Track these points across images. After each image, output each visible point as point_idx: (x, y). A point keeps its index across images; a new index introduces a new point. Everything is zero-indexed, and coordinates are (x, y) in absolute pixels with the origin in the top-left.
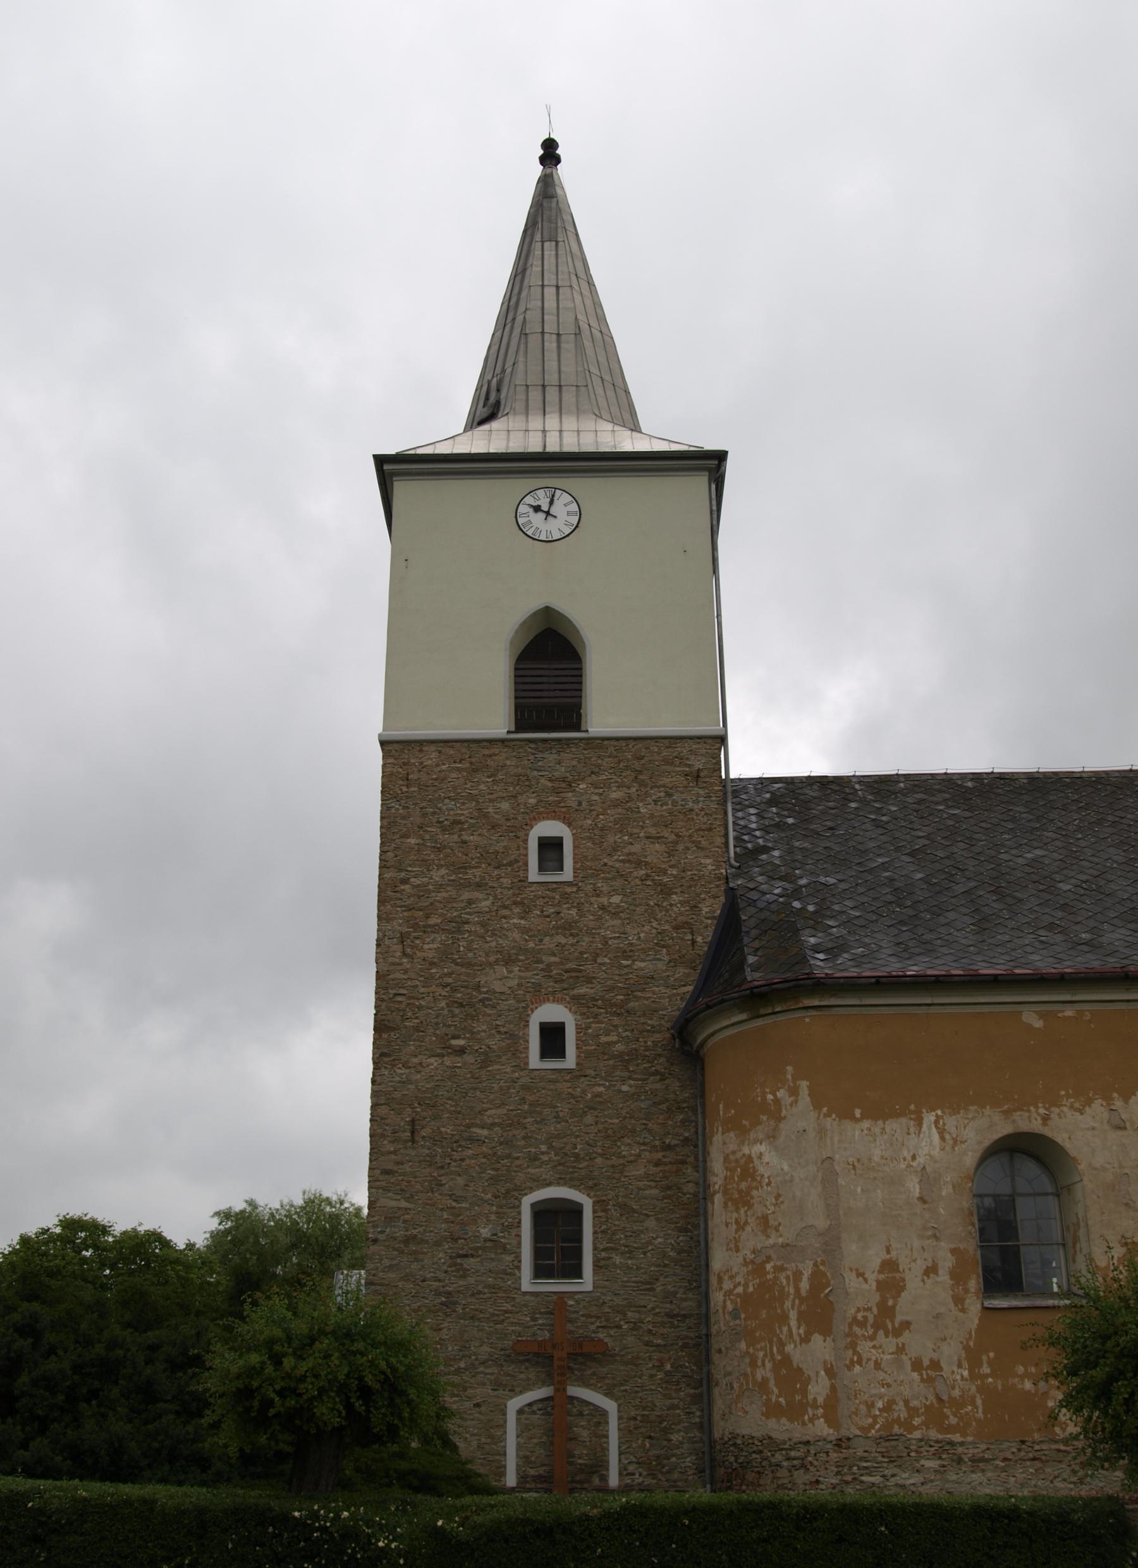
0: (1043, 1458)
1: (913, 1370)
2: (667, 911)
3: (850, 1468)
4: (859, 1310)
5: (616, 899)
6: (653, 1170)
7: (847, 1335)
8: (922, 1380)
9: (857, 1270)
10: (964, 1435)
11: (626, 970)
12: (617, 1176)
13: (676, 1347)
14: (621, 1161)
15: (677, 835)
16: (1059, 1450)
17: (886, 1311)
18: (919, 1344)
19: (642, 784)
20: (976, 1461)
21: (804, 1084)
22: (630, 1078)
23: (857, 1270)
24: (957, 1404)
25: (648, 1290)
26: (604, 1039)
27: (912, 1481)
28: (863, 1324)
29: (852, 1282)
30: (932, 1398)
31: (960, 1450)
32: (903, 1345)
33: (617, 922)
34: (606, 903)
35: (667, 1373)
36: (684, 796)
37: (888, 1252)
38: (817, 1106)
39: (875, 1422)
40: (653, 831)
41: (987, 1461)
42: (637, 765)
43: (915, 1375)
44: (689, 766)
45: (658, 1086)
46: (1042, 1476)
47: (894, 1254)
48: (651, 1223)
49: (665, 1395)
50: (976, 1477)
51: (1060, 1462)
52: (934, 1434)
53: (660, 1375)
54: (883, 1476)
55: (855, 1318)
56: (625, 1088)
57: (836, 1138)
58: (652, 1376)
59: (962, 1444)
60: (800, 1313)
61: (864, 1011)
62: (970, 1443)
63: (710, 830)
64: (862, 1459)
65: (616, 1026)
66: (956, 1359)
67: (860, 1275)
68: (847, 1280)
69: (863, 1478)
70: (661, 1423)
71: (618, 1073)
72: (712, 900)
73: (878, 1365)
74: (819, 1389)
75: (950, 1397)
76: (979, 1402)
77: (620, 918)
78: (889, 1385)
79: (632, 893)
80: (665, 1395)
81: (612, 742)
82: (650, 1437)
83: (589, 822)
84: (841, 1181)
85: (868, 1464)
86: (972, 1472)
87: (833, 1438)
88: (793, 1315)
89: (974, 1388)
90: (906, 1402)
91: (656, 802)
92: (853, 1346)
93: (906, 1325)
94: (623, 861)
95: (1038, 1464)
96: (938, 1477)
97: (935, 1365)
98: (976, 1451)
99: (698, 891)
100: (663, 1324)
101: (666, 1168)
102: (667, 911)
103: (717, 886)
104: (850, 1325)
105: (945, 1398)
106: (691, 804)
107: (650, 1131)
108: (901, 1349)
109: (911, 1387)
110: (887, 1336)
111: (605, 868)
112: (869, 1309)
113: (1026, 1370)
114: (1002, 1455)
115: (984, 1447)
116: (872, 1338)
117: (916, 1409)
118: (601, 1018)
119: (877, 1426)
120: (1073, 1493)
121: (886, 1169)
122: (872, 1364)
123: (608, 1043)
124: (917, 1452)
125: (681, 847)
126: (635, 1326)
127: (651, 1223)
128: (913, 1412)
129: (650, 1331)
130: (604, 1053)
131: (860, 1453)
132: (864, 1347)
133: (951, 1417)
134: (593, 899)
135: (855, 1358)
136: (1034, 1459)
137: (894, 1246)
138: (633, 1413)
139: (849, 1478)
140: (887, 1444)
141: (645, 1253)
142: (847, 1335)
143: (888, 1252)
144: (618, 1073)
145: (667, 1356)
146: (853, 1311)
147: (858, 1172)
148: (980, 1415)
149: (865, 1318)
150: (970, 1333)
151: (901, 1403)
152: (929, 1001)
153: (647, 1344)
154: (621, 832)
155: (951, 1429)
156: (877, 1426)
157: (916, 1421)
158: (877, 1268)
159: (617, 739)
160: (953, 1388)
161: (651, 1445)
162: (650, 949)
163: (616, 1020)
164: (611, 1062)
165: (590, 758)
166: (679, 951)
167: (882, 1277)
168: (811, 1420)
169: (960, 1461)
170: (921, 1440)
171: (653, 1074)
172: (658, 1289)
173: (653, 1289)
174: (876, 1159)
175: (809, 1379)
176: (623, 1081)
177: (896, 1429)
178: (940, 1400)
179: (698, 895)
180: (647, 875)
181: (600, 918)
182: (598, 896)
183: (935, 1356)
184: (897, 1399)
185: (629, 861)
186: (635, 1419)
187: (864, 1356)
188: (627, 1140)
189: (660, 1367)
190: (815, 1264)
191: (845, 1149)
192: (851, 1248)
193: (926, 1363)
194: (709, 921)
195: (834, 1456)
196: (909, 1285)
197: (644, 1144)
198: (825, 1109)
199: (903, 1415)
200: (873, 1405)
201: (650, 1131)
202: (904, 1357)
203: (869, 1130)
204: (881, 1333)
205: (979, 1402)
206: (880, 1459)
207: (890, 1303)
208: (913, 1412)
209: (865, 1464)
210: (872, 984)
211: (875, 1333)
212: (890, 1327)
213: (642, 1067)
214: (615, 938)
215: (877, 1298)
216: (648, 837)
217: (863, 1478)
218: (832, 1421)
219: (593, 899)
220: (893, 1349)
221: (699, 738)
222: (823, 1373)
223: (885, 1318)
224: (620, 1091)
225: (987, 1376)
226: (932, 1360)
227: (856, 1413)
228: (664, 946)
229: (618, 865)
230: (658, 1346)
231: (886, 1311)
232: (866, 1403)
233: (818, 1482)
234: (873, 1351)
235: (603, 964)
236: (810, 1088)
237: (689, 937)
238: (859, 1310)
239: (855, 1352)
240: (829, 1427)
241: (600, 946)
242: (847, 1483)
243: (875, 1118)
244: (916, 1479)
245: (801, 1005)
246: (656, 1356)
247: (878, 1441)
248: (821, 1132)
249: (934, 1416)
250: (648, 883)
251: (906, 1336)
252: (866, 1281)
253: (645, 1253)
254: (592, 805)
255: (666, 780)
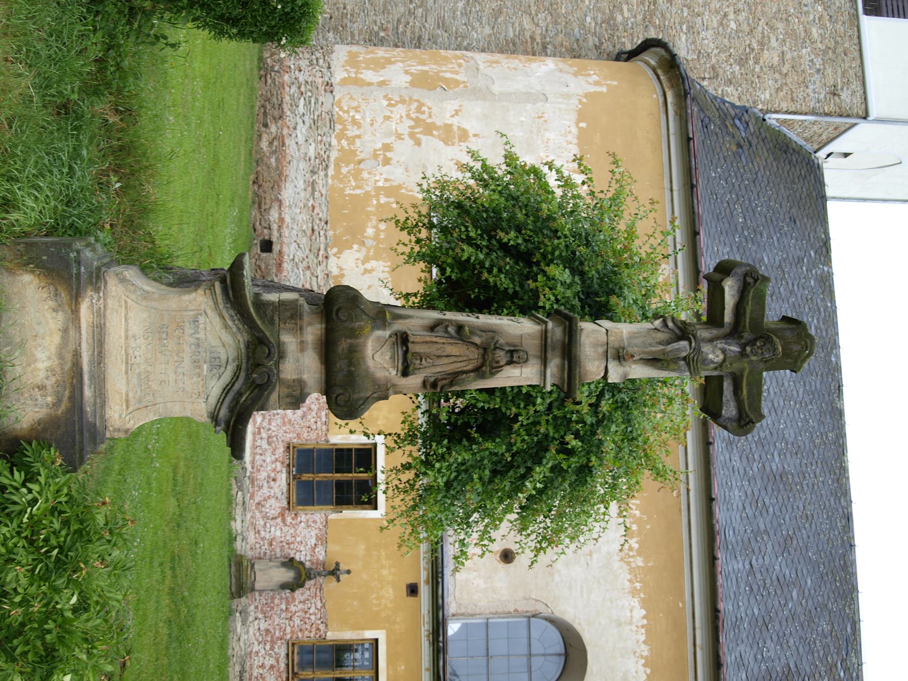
0: (314, 237)
1: (383, 144)
2: (726, 61)
3: (311, 91)
4: (430, 108)
5: (733, 25)
6: (528, 35)
7: (410, 98)
8: (375, 151)
9: (460, 110)
10: (333, 177)
11: (678, 28)
12: (522, 8)
13: (396, 40)
14: (533, 12)
15: (786, 75)
16: (319, 250)
17: (429, 129)
18: (403, 150)
19: (825, 52)
20: (313, 184)
21: (604, 89)
22: (596, 23)
23: (460, 110)
24: (357, 174)
25: (439, 24)
26: (625, 7)
27: (299, 135)
28: (419, 110)
29: (451, 105)
30: (361, 156)
31: (322, 173)
32: (403, 139)
33: (715, 24)
34: (729, 17)
35: (377, 34)
36: (818, 82)
37: (475, 135)
38: (587, 95)
39: (344, 112)
40: (788, 56)
41: (313, 194)
42: (840, 50)
43: (379, 145)
44: (842, 89)
45: (591, 43)
46: (300, 234)
47: (473, 139)
48: (487, 30)
49: (361, 30)
50: (301, 184)
51: (310, 250)
52: (334, 155)
53: (376, 28)
54: (303, 114)
55: (423, 105)
56: (588, 19)
57: (562, 106)
58: (375, 22)
59: (326, 175)
60: (427, 71)
61: (665, 139)
62: (327, 181)
63: (792, 100)
64: (317, 99)
65: (635, 17)
66: (392, 177)
67: (457, 112)
68: (453, 102)
69: (302, 99)
70: (341, 26)
71: (600, 15)
72: (737, 95)
73: (387, 118)
74: (369, 75)
75: (362, 170)
76: (358, 192)
77: (718, 27)
78: (372, 125)
79: (738, 37)
80: (361, 30)
81: (856, 33)
82: (331, 18)
83: (792, 11)
84: (529, 106)
85: (313, 104)
86: (305, 181)
87: (333, 80)
88: (425, 68)
89: (368, 189)
90: (359, 137)
91: (812, 61)
92: (403, 101)
93: (418, 143)
94: (763, 33)
95: (309, 232)
96: (302, 155)
97: (387, 161)
98: (321, 186)
99: (743, 86)
100: (413, 33)
101: (529, 44)
102: (726, 61)
103: (748, 101)
104: (418, 101)
105: (362, 166)
106: (812, 87)
107: (556, 35)
108: (399, 137)
109: (369, 142)
110: (410, 127)
111: (756, 19)
112: (430, 116)
113: (382, 231)
114: (316, 205)
115: (324, 192)
116: (408, 116)
117: (353, 143)
118: (641, 6)
119: (341, 113)
120: (286, 257)
121: (539, 142)
122: (389, 114)
123: (622, 10)
124: (321, 141)
125: (777, 76)
126: (411, 13)
127: (487, 30)
128: (352, 140)
129: (408, 23)
130: (614, 7)
131: (321, 99)
132: (401, 110)
133: (347, 169)
134: (732, 8)
135: (393, 102)
136: (313, 230)
137: (479, 140)
138: (348, 7)
139: (303, 89)
140: (328, 120)
141: (465, 24)
142: (410, 98)
143: (475, 135)
144: (600, 15)
145: (390, 34)
146: (429, 104)
147: (537, 120)
148: (348, 191)
149: (423, 113)
150: (411, 191)
151: (358, 133)
152: (675, 187)
153: (399, 21)
154: (786, 33)
155: (338, 167)
156: (341, 113)
157: (344, 143)
158: (462, 126)
159: (859, 37)
160: (369, 173)
161: (325, 18)
162: (696, 46)
163: (640, 17)
164: (608, 11)
165: (842, 15)
166: (695, 68)
167: (455, 128)
168: (346, 70)
169: (313, 172)
170: (330, 145)
171: (600, 40)
172: (439, 31)
173: (439, 27)
174: (547, 135)
175: (377, 71)
176: (594, 19)
177: (338, 127)
178: (360, 162)
179: (740, 85)
180: (753, 50)
181: (717, 12)
182: (735, 12)
183: (393, 162)
184: (361, 130)
185: (763, 37)
186: (345, 8)
187: (394, 109)
188: (549, 18)
189: (382, 28)
190: (464, 82)
191: (554, 112)
192: (477, 108)
193: (389, 155)
194: (720, 92)
195: (320, 80)
196: (449, 148)
197: (547, 30)
198: (585, 100)
199: (350, 134)
200: (357, 111)
201: (556, 35)
202: (393, 138)
203: (570, 132)
204: (412, 123)
205: (358, 192)
206: (317, 113)
207: (435, 132)
208: (352, 140)
209: (313, 101)
210: (688, 134)
211: (412, 119)
212: (416, 130)
213: (605, 33)
214: (703, 22)
215: (439, 123)
216: (783, 53)
217: (302, 99)
218: (344, 82)
219: (732, 8)
220: (400, 131)
221: (865, 99)
222: (382, 79)
223: (423, 128)
224: (586, 16)
225: (378, 200)
226: (390, 159)
227: (351, 98)
228: (698, 57)
229: (760, 29)
230: (397, 28)
231: (429, 129)
232: (359, 107)
233: (300, 70)
234: (398, 116)
235: (682, 11)
236: (601, 93)
237: (707, 76)
238: (430, 108)
239: (397, 102)
240: (342, 80)
241: (696, 10)
242: (299, 88)
243: (579, 138)
244: (301, 139)
245: (666, 90)
246: (390, 26)
247: (330, 113)
248: (568, 96)
249: (348, 156)
250: (748, 50)
251: (409, 142)
252: (452, 116)
253: (465, 24)
254: (805, 14)
255: (829, 71)
